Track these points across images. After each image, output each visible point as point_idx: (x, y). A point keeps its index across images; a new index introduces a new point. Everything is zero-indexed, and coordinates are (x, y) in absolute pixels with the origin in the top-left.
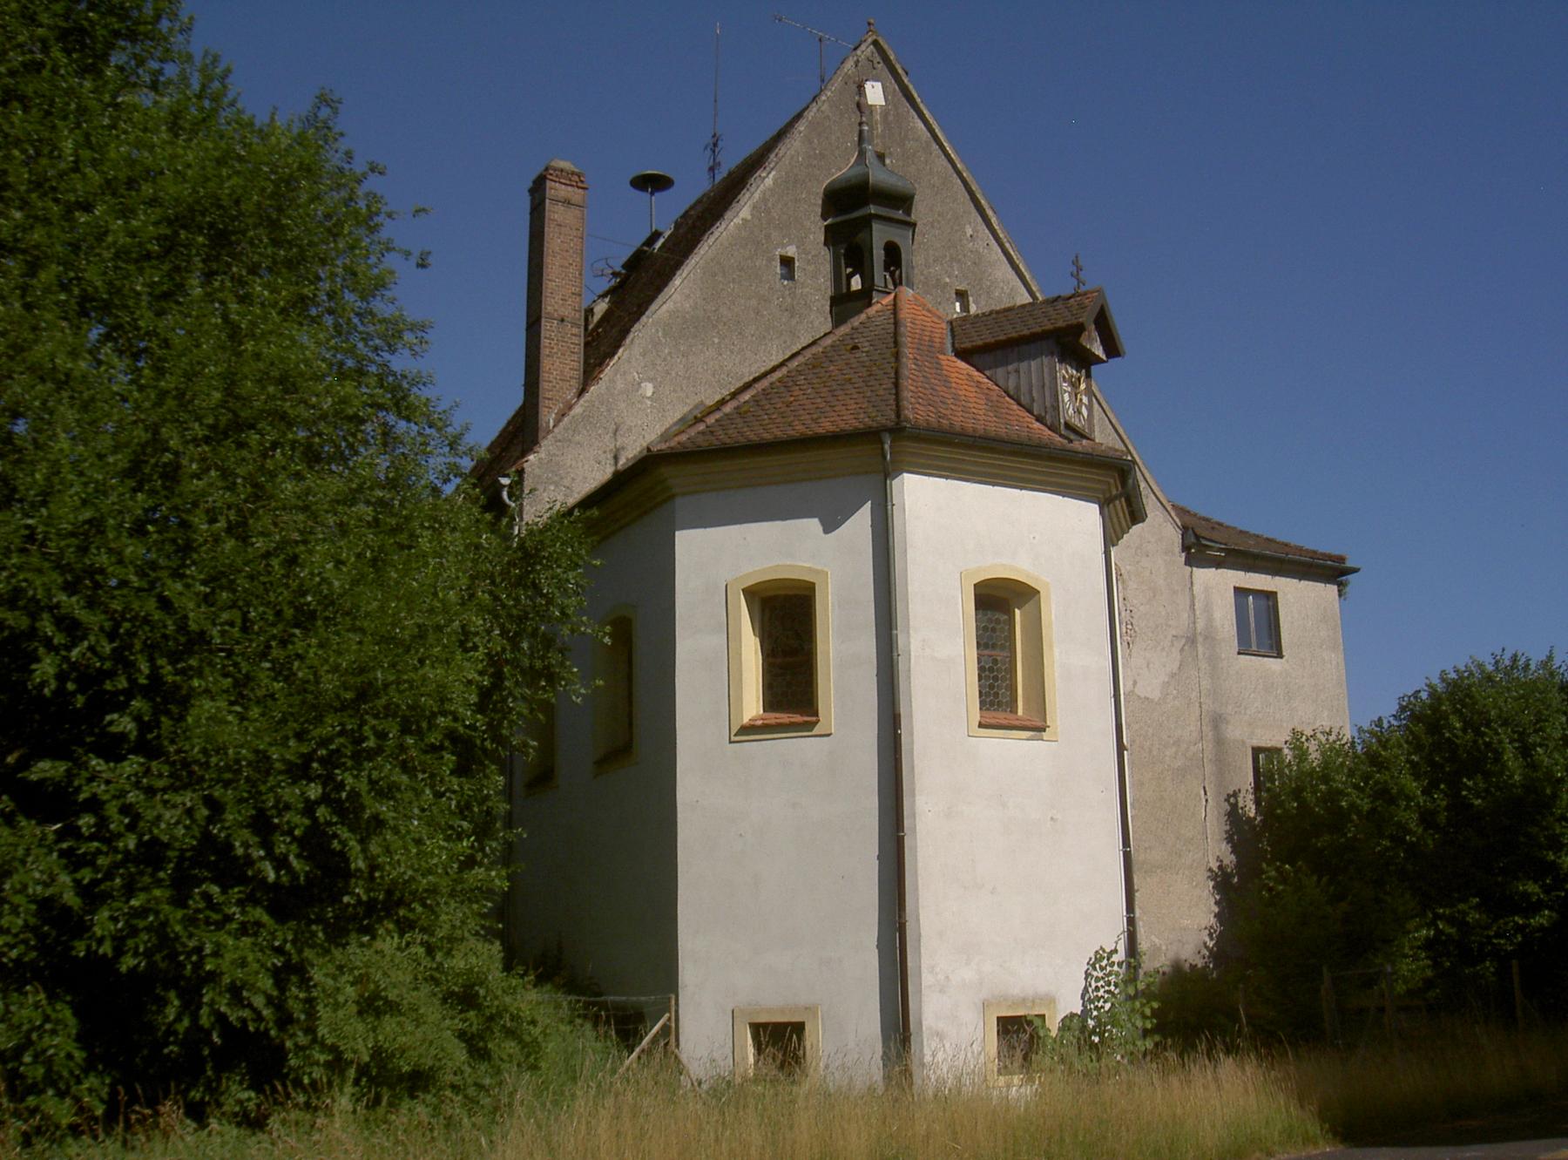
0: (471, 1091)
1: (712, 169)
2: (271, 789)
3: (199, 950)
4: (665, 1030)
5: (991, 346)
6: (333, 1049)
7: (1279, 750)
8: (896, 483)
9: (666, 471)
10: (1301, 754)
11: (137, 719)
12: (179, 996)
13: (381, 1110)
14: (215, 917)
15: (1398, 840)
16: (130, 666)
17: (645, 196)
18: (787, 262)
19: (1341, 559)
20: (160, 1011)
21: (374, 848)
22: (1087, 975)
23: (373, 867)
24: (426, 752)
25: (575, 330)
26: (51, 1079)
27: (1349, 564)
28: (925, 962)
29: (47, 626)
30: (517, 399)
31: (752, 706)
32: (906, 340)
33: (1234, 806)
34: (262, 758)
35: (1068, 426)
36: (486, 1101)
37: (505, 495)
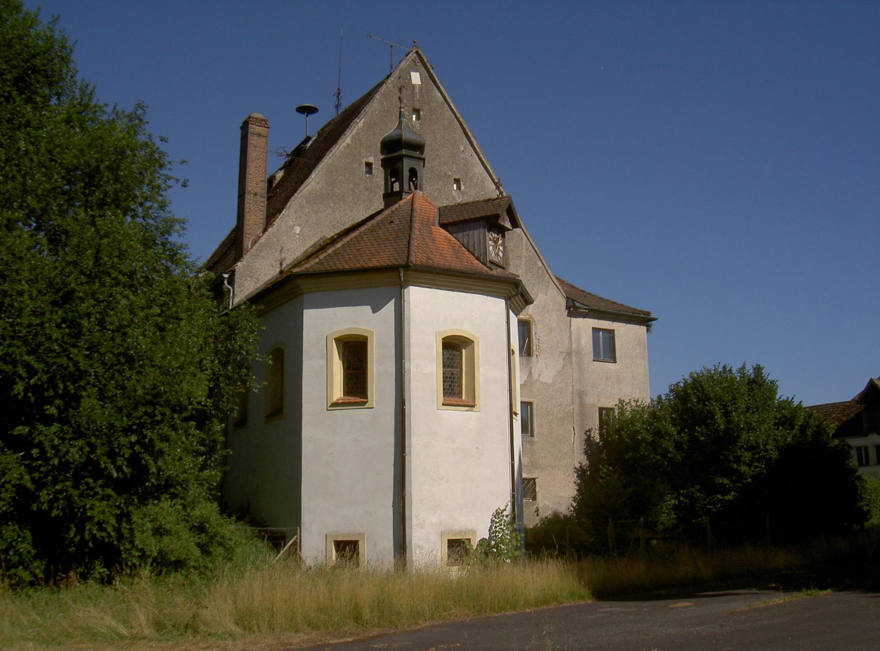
0: (202, 569)
1: (337, 106)
2: (116, 439)
3: (84, 506)
4: (295, 543)
5: (459, 221)
6: (142, 550)
7: (613, 409)
9: (299, 282)
11: (58, 408)
12: (75, 526)
13: (162, 577)
14: (92, 493)
16: (55, 387)
17: (303, 116)
18: (369, 165)
19: (649, 314)
20: (67, 532)
21: (160, 463)
22: (492, 521)
23: (159, 469)
24: (183, 421)
25: (262, 200)
26: (21, 562)
27: (652, 316)
28: (414, 513)
29: (21, 371)
30: (233, 223)
31: (338, 393)
32: (416, 219)
34: (111, 426)
35: (491, 262)
36: (209, 573)
37: (226, 282)
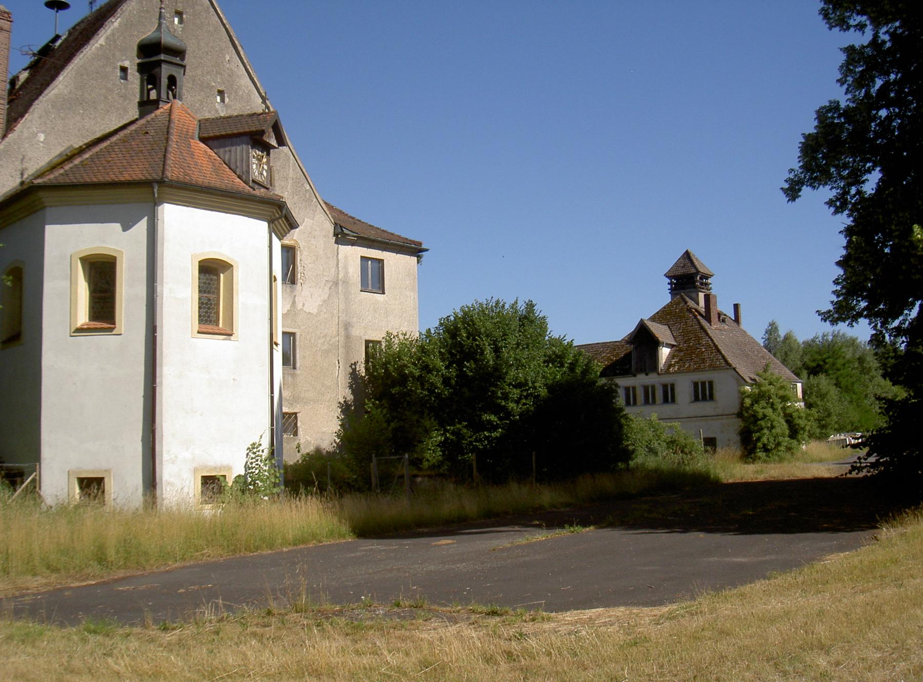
4: (34, 480)
5: (221, 136)
7: (380, 342)
8: (160, 208)
9: (41, 194)
10: (389, 346)
15: (431, 392)
18: (124, 70)
19: (420, 244)
27: (424, 247)
31: (83, 317)
32: (174, 131)
33: (354, 370)
35: (254, 181)
